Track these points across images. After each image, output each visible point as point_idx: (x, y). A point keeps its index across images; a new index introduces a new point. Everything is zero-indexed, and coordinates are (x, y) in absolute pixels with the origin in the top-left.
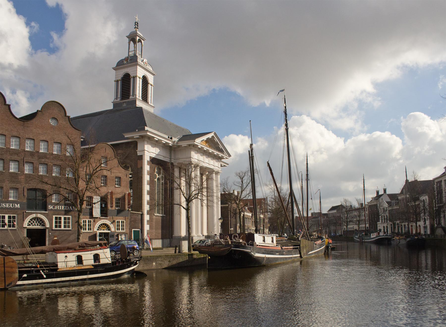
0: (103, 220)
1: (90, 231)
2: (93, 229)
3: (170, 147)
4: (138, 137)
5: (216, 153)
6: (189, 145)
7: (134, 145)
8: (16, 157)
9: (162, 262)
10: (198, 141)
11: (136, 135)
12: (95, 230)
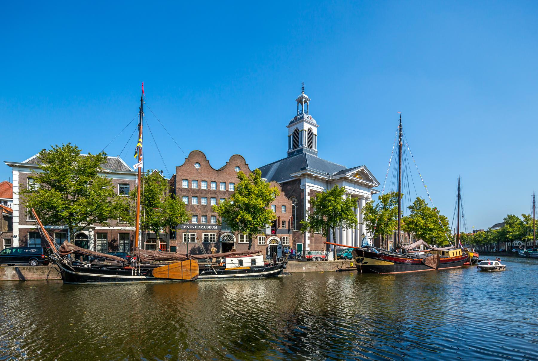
0: (273, 237)
1: (263, 244)
2: (266, 243)
3: (327, 181)
4: (300, 175)
5: (366, 182)
6: (341, 178)
7: (297, 181)
8: (214, 195)
9: (310, 267)
10: (349, 175)
11: (299, 174)
12: (268, 243)
